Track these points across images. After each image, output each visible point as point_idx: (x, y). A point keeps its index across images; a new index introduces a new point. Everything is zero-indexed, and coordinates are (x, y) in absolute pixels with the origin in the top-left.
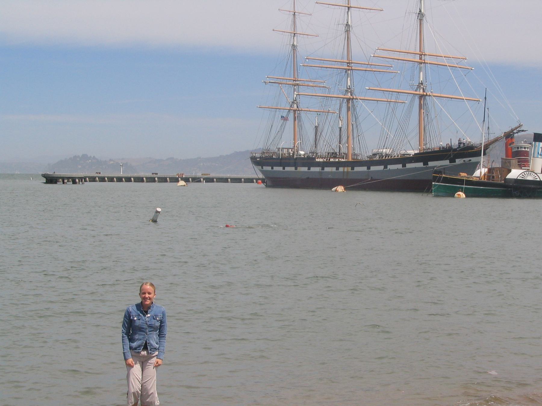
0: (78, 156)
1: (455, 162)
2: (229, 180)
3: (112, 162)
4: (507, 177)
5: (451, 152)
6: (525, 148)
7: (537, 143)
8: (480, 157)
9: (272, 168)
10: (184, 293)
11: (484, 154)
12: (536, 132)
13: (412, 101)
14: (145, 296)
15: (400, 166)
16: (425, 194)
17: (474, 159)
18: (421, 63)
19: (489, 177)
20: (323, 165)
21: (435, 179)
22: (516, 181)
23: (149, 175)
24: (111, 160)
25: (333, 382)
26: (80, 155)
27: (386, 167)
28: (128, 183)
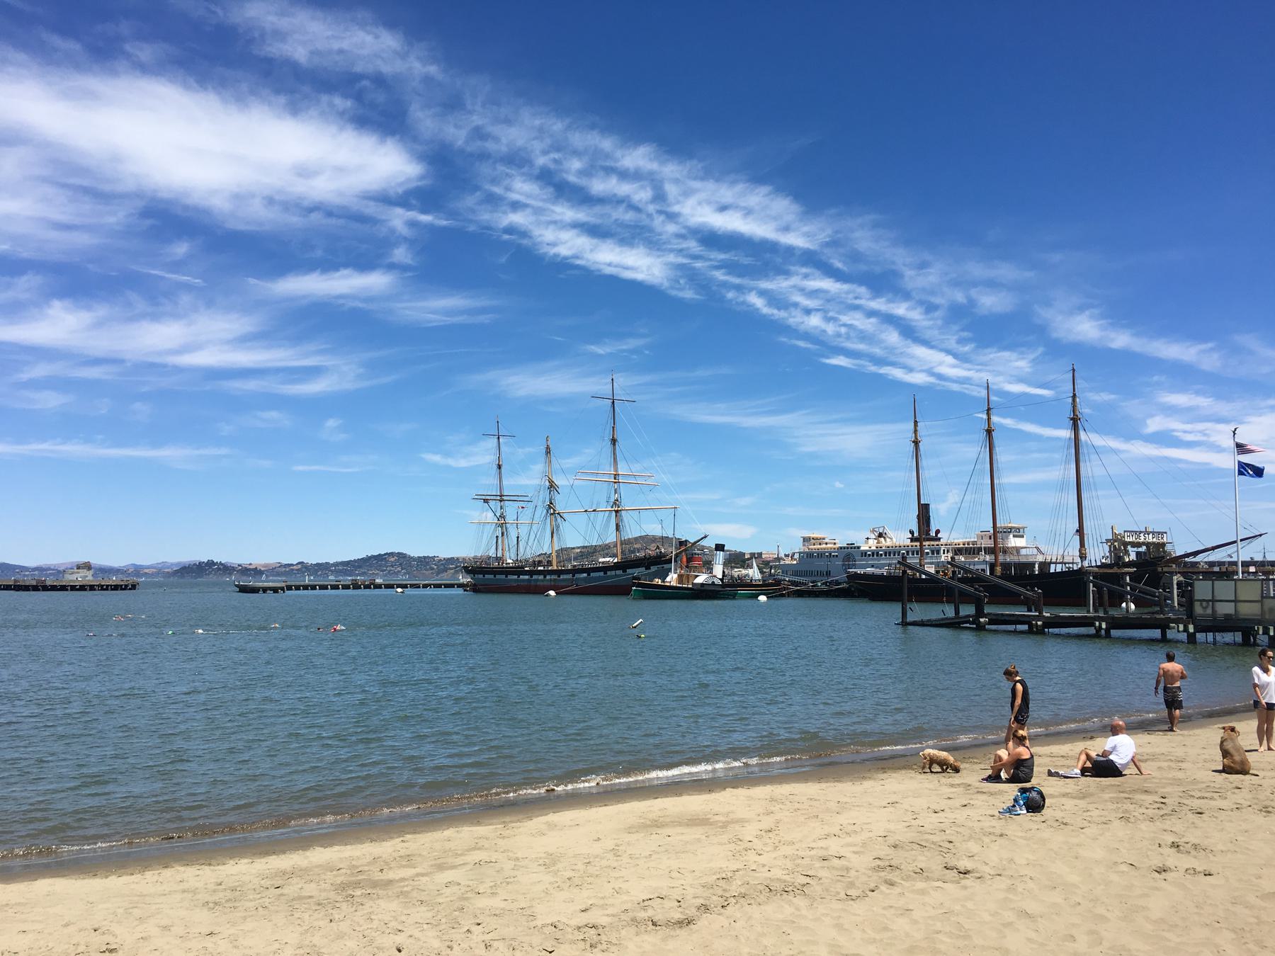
0: (199, 563)
1: (650, 569)
2: (329, 587)
3: (240, 568)
4: (694, 582)
5: (646, 561)
6: (698, 554)
7: (718, 552)
8: (670, 565)
9: (484, 576)
10: (964, 864)
11: (676, 561)
12: (717, 543)
13: (610, 516)
14: (1089, 948)
15: (602, 574)
16: (807, 599)
17: (666, 566)
18: (615, 482)
19: (764, 581)
20: (531, 573)
21: (634, 584)
22: (702, 585)
23: (34, 583)
24: (239, 565)
25: (230, 720)
26: (206, 561)
27: (589, 575)
28: (661, 601)
